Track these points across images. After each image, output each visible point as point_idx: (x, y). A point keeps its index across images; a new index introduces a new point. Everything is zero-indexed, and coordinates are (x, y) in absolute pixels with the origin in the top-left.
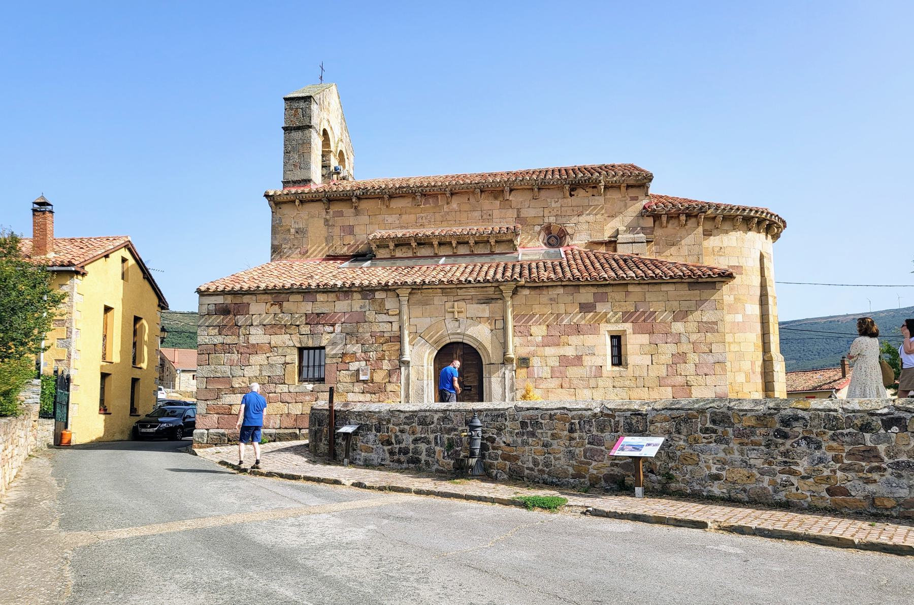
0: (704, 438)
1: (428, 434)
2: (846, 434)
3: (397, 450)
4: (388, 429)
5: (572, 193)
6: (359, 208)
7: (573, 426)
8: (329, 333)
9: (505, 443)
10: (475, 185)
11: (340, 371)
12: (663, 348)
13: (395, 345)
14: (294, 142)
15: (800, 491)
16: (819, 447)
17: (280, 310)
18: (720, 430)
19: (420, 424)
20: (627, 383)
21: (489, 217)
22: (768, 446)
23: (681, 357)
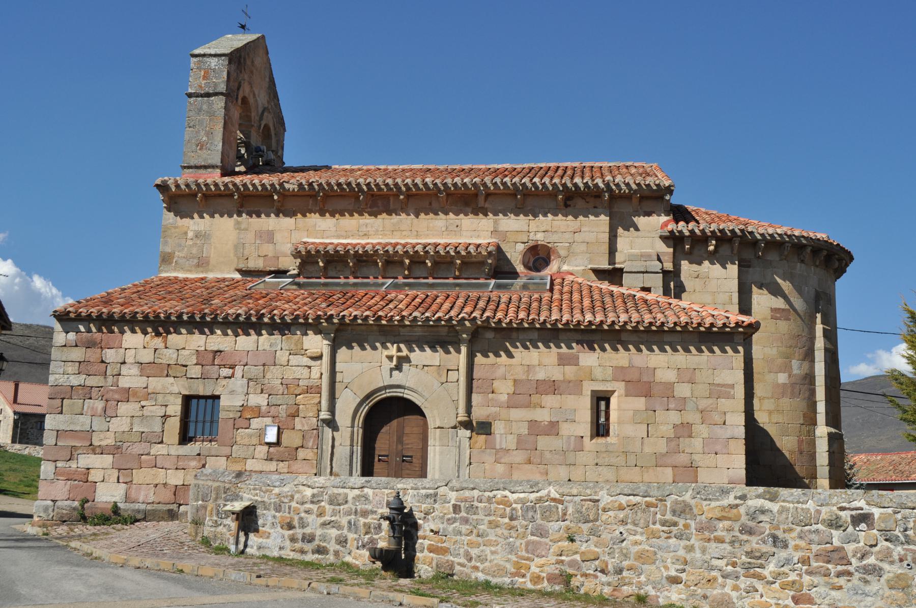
0: (663, 531)
2: (814, 531)
3: (300, 537)
4: (290, 508)
5: (568, 203)
7: (514, 512)
8: (225, 378)
9: (432, 531)
12: (660, 415)
13: (314, 397)
15: (764, 599)
16: (786, 546)
17: (164, 345)
18: (681, 522)
19: (331, 503)
20: (613, 461)
21: (456, 229)
22: (732, 543)
23: (684, 430)
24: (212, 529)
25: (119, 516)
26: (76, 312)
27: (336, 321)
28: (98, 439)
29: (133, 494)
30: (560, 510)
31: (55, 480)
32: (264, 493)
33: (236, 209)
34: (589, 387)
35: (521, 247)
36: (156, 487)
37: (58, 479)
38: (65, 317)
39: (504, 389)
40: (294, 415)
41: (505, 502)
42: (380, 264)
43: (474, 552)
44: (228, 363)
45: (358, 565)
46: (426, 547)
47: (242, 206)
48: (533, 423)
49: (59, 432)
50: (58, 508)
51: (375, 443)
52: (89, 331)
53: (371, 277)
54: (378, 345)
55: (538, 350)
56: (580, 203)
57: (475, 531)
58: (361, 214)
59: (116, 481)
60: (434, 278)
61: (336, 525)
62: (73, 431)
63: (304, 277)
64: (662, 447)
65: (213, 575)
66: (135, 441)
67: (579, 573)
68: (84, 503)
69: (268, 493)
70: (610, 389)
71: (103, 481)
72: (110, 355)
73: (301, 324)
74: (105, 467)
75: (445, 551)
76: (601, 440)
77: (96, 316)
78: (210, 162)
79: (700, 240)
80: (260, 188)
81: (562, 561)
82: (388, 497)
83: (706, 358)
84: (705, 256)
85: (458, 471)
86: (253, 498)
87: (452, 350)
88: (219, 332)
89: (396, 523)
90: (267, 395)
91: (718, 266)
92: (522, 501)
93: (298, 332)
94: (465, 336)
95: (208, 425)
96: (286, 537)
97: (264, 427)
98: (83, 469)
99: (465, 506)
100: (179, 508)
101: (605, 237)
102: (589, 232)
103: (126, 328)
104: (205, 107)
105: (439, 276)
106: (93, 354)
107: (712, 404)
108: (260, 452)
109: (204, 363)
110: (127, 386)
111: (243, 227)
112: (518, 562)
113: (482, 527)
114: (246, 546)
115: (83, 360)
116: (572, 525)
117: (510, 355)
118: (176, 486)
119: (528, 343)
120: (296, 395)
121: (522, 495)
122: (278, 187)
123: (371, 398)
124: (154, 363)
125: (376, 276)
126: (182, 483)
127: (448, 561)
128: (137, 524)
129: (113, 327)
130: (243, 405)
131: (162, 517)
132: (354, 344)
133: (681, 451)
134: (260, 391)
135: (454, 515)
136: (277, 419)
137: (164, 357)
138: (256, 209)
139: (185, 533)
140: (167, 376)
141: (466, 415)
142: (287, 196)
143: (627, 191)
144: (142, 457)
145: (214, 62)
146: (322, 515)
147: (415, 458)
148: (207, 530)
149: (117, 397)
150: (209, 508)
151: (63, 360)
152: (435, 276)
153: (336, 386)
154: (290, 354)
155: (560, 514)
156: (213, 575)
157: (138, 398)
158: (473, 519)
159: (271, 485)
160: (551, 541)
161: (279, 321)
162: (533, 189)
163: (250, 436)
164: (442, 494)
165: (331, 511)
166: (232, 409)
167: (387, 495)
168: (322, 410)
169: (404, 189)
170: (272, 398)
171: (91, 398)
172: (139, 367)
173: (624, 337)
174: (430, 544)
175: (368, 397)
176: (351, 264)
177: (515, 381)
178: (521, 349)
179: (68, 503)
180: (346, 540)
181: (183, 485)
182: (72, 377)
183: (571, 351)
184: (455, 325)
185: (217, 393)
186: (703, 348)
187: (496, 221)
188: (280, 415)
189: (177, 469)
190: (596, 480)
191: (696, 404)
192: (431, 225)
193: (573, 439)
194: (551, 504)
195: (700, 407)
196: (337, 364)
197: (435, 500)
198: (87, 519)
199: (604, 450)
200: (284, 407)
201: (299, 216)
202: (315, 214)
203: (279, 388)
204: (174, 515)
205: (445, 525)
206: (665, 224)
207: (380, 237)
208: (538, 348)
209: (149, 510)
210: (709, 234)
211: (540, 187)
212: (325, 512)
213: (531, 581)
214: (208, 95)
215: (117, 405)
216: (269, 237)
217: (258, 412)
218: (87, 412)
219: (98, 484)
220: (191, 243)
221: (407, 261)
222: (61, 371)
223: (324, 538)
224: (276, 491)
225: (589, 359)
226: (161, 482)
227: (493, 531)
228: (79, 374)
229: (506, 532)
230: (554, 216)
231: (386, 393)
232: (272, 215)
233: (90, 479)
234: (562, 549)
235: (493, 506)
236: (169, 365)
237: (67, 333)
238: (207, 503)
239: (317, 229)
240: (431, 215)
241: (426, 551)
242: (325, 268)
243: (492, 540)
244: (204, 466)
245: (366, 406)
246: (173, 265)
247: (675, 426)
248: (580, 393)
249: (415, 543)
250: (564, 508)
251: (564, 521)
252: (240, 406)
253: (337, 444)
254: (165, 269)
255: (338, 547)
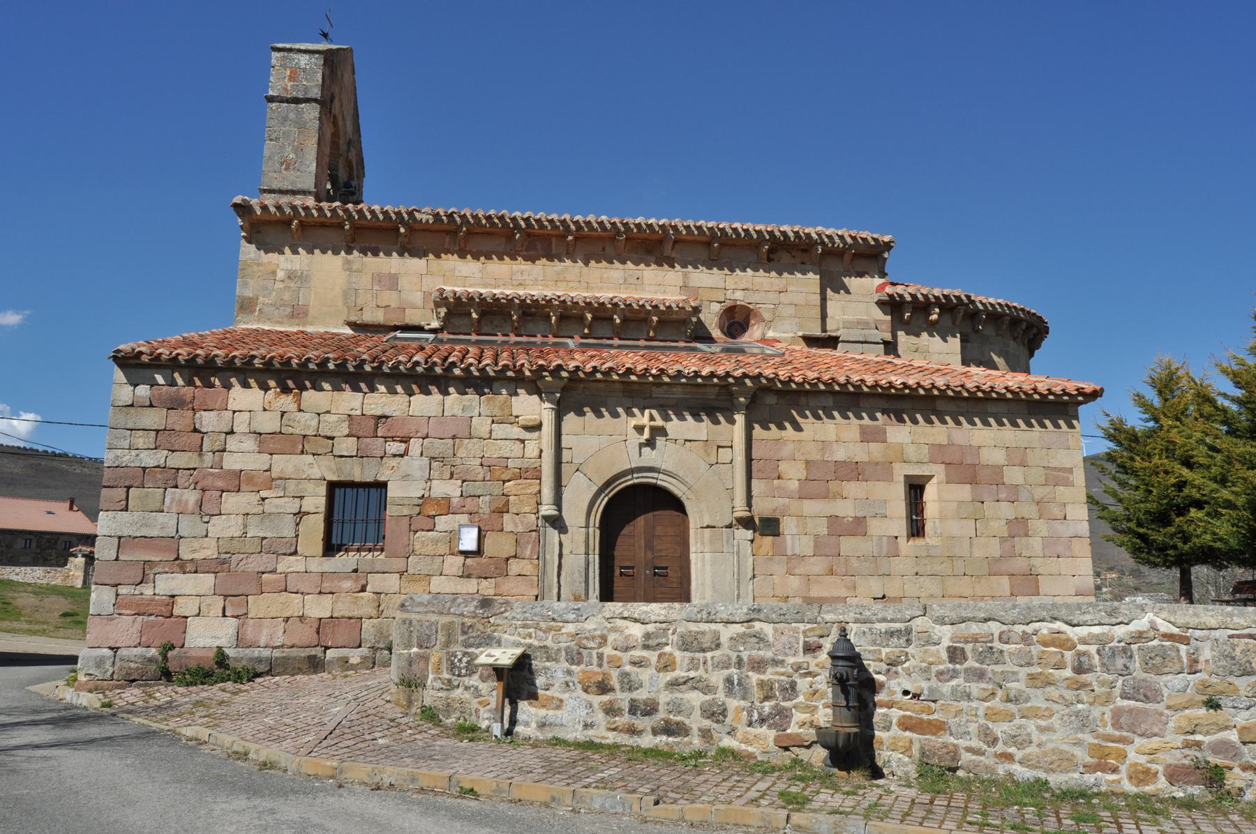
1: (706, 671)
3: (626, 706)
4: (600, 657)
5: (771, 256)
8: (395, 456)
9: (906, 693)
11: (416, 532)
13: (531, 485)
17: (296, 406)
19: (685, 646)
20: (937, 568)
21: (636, 282)
23: (1019, 527)
24: (440, 695)
25: (228, 669)
26: (151, 354)
27: (564, 374)
28: (190, 549)
29: (249, 634)
30: (1183, 654)
31: (116, 616)
32: (545, 632)
33: (345, 244)
34: (901, 471)
35: (716, 308)
36: (287, 621)
37: (120, 614)
38: (131, 361)
39: (794, 473)
40: (502, 510)
41: (1060, 642)
42: (554, 318)
43: (999, 729)
44: (398, 434)
45: (754, 753)
46: (894, 721)
47: (353, 241)
48: (833, 519)
49: (122, 540)
50: (121, 660)
51: (614, 549)
52: (173, 383)
53: (550, 336)
54: (620, 410)
55: (834, 421)
56: (785, 257)
57: (1000, 693)
58: (513, 258)
59: (221, 615)
60: (620, 339)
61: (700, 685)
62: (146, 537)
63: (449, 333)
64: (995, 549)
65: (548, 799)
66: (251, 552)
67: (1237, 764)
68: (167, 651)
69: (553, 632)
70: (926, 473)
71: (198, 615)
72: (208, 420)
73: (510, 379)
74: (202, 593)
75: (938, 727)
76: (919, 542)
77: (185, 360)
78: (299, 186)
79: (921, 307)
80: (381, 217)
81: (1198, 744)
82: (805, 636)
83: (1038, 434)
84: (924, 326)
85: (738, 587)
86: (523, 641)
87: (721, 419)
88: (382, 388)
89: (851, 682)
90: (460, 482)
91: (937, 338)
92: (1101, 641)
93: (504, 391)
94: (742, 399)
95: (372, 527)
96: (596, 705)
97: (457, 528)
98: (164, 597)
99: (974, 650)
100: (325, 653)
101: (817, 299)
102: (797, 292)
103: (233, 380)
104: (292, 116)
105: (628, 337)
106: (179, 420)
107: (1049, 493)
108: (451, 565)
109: (361, 434)
110: (237, 467)
111: (354, 267)
112: (1101, 746)
113: (1014, 685)
114: (513, 722)
115: (163, 427)
116: (1214, 679)
117: (798, 428)
118: (320, 619)
119: (820, 412)
120: (504, 482)
121: (1097, 630)
122: (406, 216)
123: (614, 485)
124: (280, 433)
125: (545, 334)
126: (329, 615)
127: (945, 745)
128: (259, 680)
129: (212, 379)
130: (423, 496)
131: (299, 668)
132: (586, 409)
133: (1017, 554)
134: (449, 476)
135: (951, 666)
136: (477, 516)
137: (296, 424)
138: (373, 245)
139: (387, 702)
140: (302, 452)
141: (747, 509)
142: (416, 230)
143: (841, 245)
144: (264, 576)
145: (303, 60)
146: (669, 668)
147: (671, 570)
148: (430, 696)
149: (220, 484)
150: (433, 660)
151: (128, 427)
152: (623, 337)
153: (563, 469)
154: (493, 422)
155: (1185, 660)
156: (548, 799)
157: (254, 485)
158: (994, 673)
159: (559, 619)
160: (1169, 707)
161: (477, 374)
162: (734, 236)
163: (436, 542)
164: (920, 629)
165: (687, 661)
166: (406, 502)
167: (804, 632)
168: (544, 502)
169: (573, 227)
170: (467, 485)
171: (176, 487)
172: (256, 439)
173: (940, 405)
174: (904, 716)
175: (608, 484)
176: (515, 318)
177: (807, 462)
178: (811, 419)
179: (139, 650)
180: (725, 710)
181: (332, 617)
182: (144, 454)
183: (875, 423)
184: (732, 384)
185: (382, 479)
186: (1033, 421)
188: (481, 511)
189: (320, 593)
190: (917, 595)
191: (1030, 492)
192: (605, 275)
193: (885, 538)
194: (1164, 643)
195: (1036, 497)
196: (563, 437)
197: (907, 640)
198: (172, 676)
199: (924, 554)
200: (487, 498)
201: (431, 256)
202: (453, 255)
203: (477, 471)
204: (318, 664)
205: (934, 682)
206: (881, 288)
207: (540, 288)
208: (833, 418)
209: (277, 658)
210: (933, 300)
211: (743, 234)
212: (674, 663)
213: (1130, 778)
214: (296, 101)
215: (221, 496)
216: (392, 282)
217: (446, 507)
218: (170, 508)
219: (189, 619)
220: (282, 286)
221: (589, 316)
222: (126, 444)
223: (677, 708)
224: (570, 628)
225: (900, 434)
226: (296, 614)
227: (1039, 692)
228: (156, 448)
229: (1069, 694)
230: (754, 271)
231: (633, 478)
232: (395, 254)
233: (176, 612)
234: (1195, 722)
235: (1036, 649)
236: (304, 436)
237: (136, 385)
238: (428, 651)
239: (457, 274)
240: (604, 263)
241: (895, 727)
242: (479, 321)
243: (1039, 708)
244: (363, 589)
245: (605, 497)
246: (257, 313)
247: (1009, 522)
248: (889, 478)
249: (871, 715)
250: (1192, 651)
251: (1195, 673)
252: (419, 498)
253: (565, 551)
254: (244, 320)
255: (707, 723)
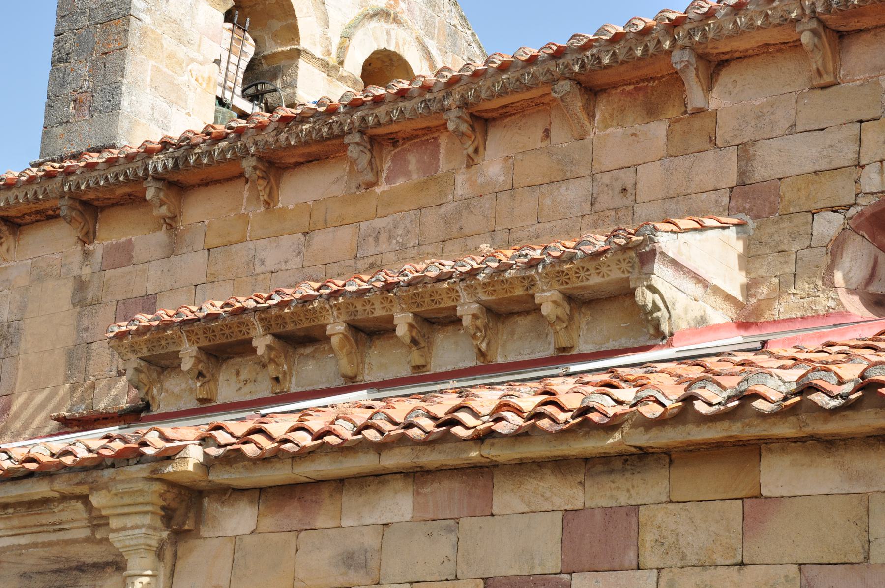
6: (181, 226)
10: (551, 65)
14: (84, 21)
21: (619, 201)
138: (123, 239)
187: (746, 151)
192: (548, 201)
